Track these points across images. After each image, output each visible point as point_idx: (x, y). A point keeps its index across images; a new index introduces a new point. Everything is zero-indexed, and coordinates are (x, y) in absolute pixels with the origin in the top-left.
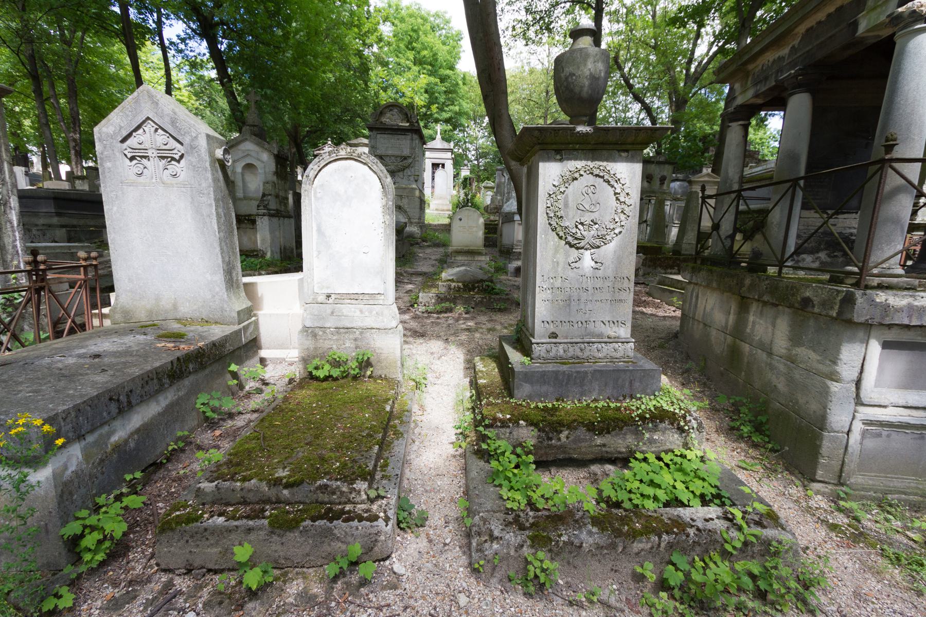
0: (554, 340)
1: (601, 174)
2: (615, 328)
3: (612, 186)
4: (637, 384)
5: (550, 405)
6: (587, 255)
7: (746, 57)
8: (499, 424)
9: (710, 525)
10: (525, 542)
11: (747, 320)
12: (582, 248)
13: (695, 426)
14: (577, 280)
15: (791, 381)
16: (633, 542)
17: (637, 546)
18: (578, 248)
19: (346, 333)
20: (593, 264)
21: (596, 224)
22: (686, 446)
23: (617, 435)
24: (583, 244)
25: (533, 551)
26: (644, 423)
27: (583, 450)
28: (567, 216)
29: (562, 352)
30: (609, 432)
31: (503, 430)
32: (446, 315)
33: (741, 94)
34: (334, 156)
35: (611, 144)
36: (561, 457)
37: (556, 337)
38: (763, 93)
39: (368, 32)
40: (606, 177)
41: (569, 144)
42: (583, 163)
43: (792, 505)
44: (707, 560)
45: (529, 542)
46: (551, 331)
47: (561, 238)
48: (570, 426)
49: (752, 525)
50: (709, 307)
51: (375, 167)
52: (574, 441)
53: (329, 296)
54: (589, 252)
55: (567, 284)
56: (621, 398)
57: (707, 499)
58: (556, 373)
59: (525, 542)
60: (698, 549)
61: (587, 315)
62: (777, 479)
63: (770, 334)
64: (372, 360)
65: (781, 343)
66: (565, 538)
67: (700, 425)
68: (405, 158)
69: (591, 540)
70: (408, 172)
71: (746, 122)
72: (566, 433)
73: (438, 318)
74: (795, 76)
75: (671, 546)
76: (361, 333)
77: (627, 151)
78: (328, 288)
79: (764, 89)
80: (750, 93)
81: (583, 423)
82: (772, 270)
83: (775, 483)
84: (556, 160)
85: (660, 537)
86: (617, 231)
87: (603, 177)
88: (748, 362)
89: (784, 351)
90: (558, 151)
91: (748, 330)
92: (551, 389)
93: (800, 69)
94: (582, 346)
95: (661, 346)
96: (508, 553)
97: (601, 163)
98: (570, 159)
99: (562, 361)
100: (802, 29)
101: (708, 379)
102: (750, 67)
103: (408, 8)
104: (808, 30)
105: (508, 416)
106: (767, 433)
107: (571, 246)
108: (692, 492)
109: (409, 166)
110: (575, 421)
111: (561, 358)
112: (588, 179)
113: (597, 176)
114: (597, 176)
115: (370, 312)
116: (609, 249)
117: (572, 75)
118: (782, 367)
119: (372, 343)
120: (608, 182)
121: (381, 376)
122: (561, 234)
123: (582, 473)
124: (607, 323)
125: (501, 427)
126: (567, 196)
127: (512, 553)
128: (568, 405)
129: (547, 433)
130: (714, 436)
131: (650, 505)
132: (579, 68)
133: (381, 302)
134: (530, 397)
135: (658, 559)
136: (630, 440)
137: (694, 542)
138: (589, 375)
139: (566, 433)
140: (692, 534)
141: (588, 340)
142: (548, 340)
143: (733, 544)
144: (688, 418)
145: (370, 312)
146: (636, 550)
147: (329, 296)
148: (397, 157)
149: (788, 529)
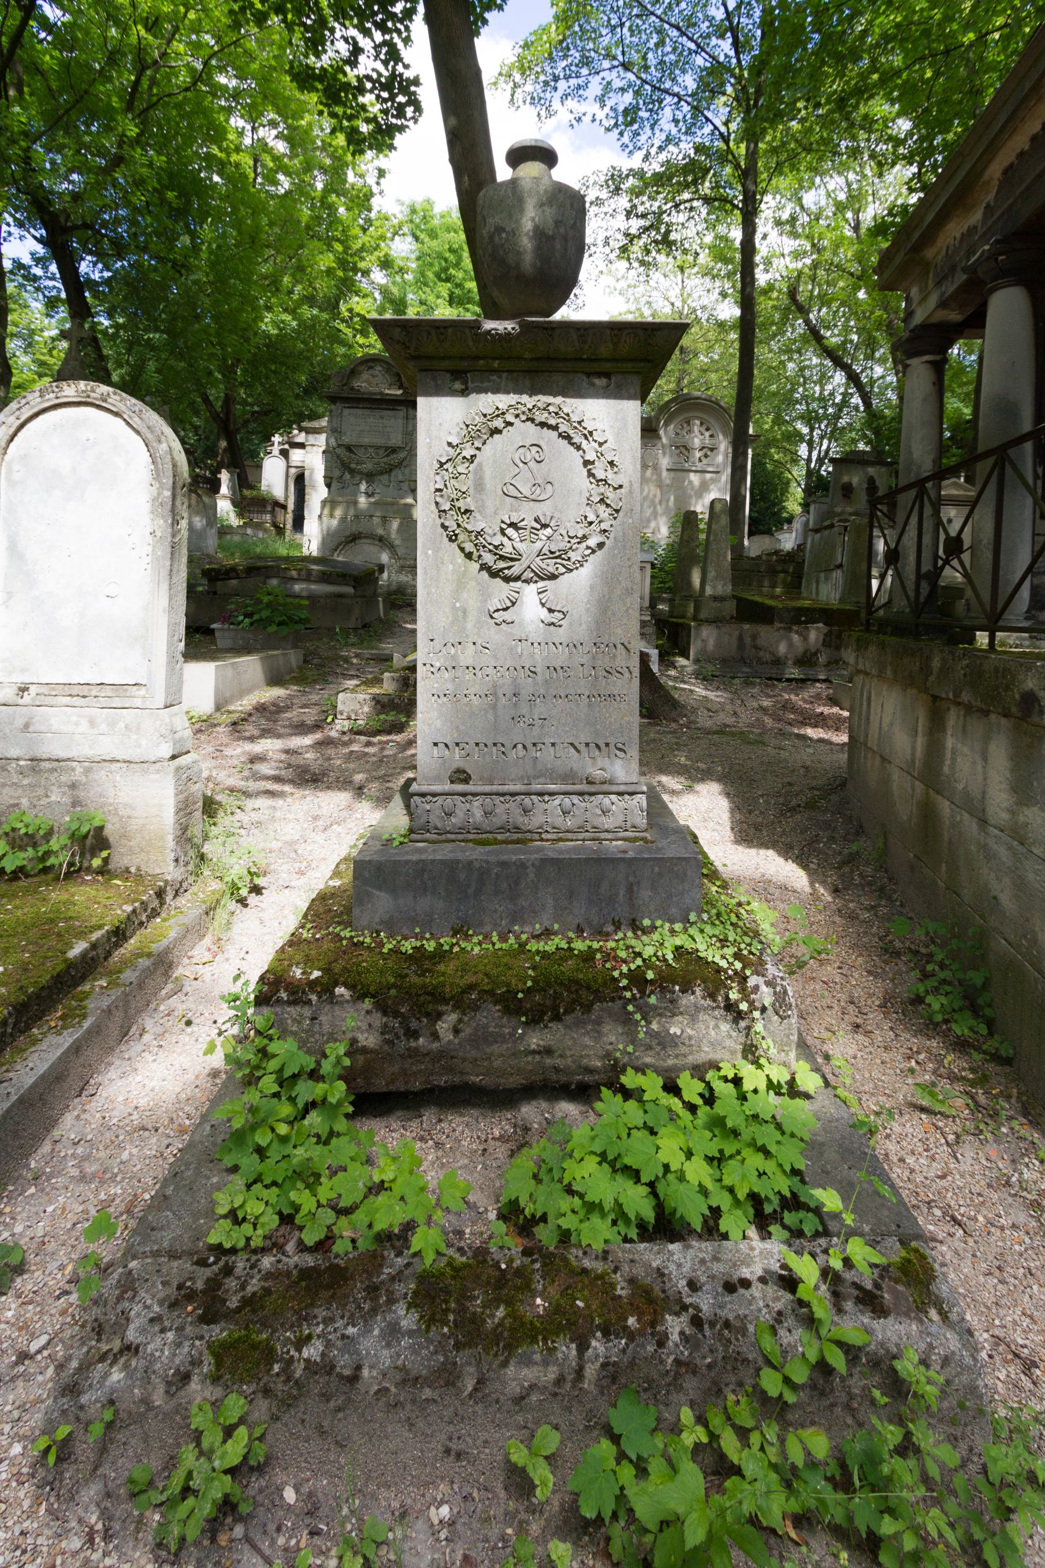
0: (460, 787)
1: (552, 422)
2: (601, 762)
3: (578, 448)
4: (645, 894)
5: (430, 946)
6: (530, 593)
7: (917, 235)
8: (284, 995)
9: (732, 1308)
10: (196, 1362)
11: (943, 746)
12: (517, 579)
13: (768, 1001)
14: (511, 649)
15: (1021, 886)
16: (505, 1364)
17: (518, 1376)
18: (507, 579)
19: (54, 770)
20: (544, 613)
21: (545, 526)
22: (751, 1052)
23: (578, 1024)
24: (517, 569)
25: (218, 1392)
26: (642, 992)
27: (497, 1063)
28: (482, 509)
29: (478, 814)
30: (557, 1018)
31: (293, 1011)
32: (384, 738)
33: (920, 303)
34: (51, 399)
35: (565, 360)
36: (442, 1081)
37: (466, 780)
38: (951, 296)
39: (363, 249)
40: (562, 428)
41: (477, 358)
42: (511, 399)
43: (1022, 1218)
44: (716, 1421)
45: (208, 1360)
46: (455, 766)
47: (469, 556)
48: (460, 1001)
49: (849, 1305)
50: (886, 720)
51: (136, 421)
52: (475, 1040)
53: (23, 689)
54: (533, 587)
55: (487, 659)
56: (610, 928)
57: (768, 1209)
58: (451, 866)
59: (196, 1362)
60: (690, 1383)
61: (536, 731)
62: (998, 1139)
63: (980, 777)
64: (109, 831)
65: (999, 800)
66: (312, 1352)
67: (781, 997)
68: (394, 450)
69: (386, 1358)
70: (398, 475)
71: (938, 358)
72: (453, 1017)
73: (368, 744)
74: (993, 256)
75: (613, 1375)
76: (87, 771)
77: (607, 375)
78: (23, 671)
79: (951, 290)
80: (933, 301)
81: (491, 993)
82: (982, 639)
83: (992, 1150)
84: (453, 393)
85: (583, 1347)
86: (592, 542)
87: (555, 428)
88: (950, 842)
89: (1005, 816)
90: (458, 374)
91: (946, 769)
92: (440, 905)
93: (997, 241)
94: (527, 801)
95: (811, 805)
96: (146, 1401)
97: (550, 399)
98: (480, 391)
99: (481, 837)
100: (995, 170)
101: (890, 879)
102: (929, 253)
103: (443, 217)
104: (1005, 172)
105: (316, 974)
106: (988, 1011)
107: (494, 574)
108: (731, 1190)
109: (400, 465)
110: (471, 987)
111: (479, 830)
112: (524, 432)
113: (543, 425)
114: (543, 425)
115: (112, 724)
116: (579, 584)
117: (500, 230)
118: (1003, 852)
119: (111, 792)
120: (568, 438)
121: (127, 870)
122: (469, 547)
123: (498, 1125)
124: (582, 748)
125: (290, 1003)
126: (480, 465)
127: (158, 1399)
128: (474, 947)
129: (405, 1021)
130: (875, 1017)
131: (598, 1233)
132: (510, 216)
133: (138, 702)
134: (391, 927)
135: (578, 1417)
136: (613, 1037)
137: (678, 1362)
138: (531, 871)
139: (453, 1017)
140: (675, 1337)
141: (537, 787)
142: (448, 787)
143: (788, 1370)
144: (752, 981)
145: (112, 724)
146: (514, 1389)
147: (23, 689)
148: (378, 448)
149: (954, 1317)
